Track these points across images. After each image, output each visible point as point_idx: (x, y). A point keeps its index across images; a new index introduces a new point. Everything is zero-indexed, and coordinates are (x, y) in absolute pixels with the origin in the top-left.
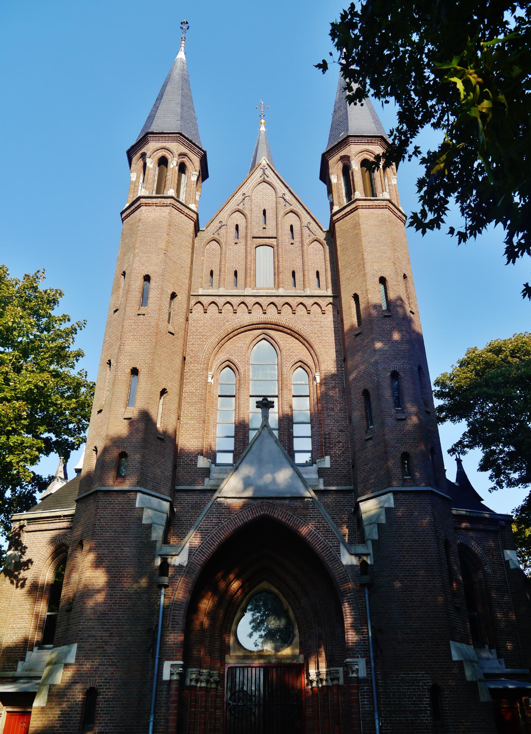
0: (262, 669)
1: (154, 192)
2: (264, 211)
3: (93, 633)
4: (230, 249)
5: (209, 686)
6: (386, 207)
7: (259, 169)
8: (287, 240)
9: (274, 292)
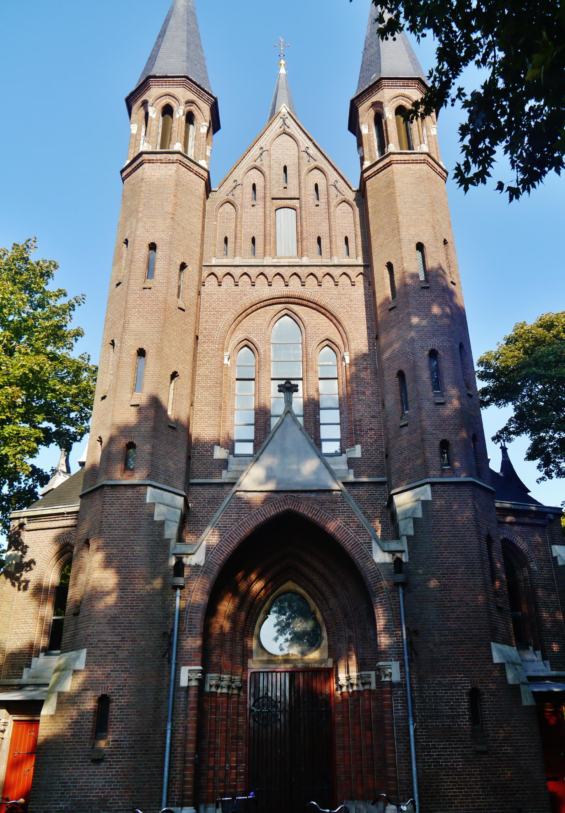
0: (287, 674)
1: (158, 147)
2: (285, 168)
3: (104, 637)
4: (247, 212)
8: (311, 201)
9: (297, 261)
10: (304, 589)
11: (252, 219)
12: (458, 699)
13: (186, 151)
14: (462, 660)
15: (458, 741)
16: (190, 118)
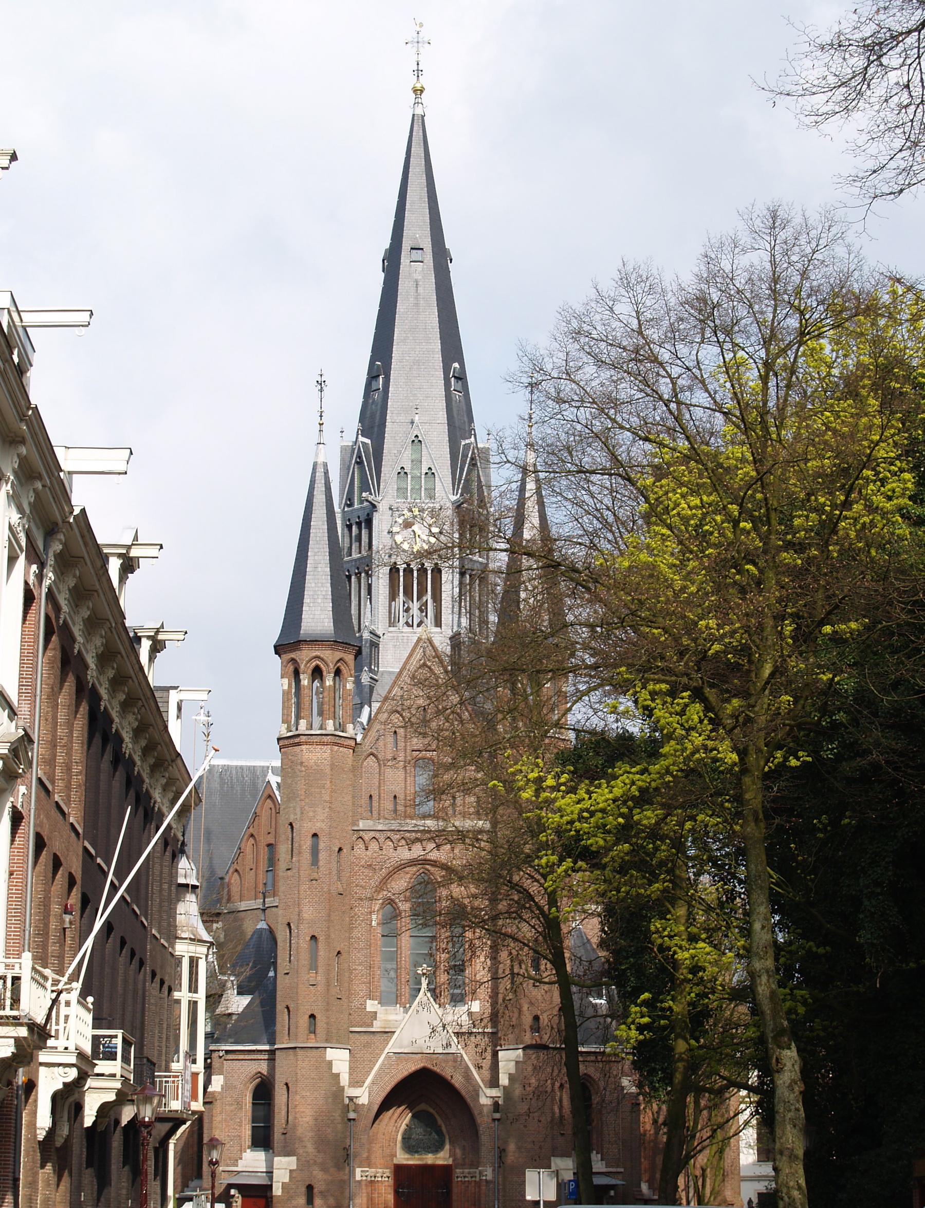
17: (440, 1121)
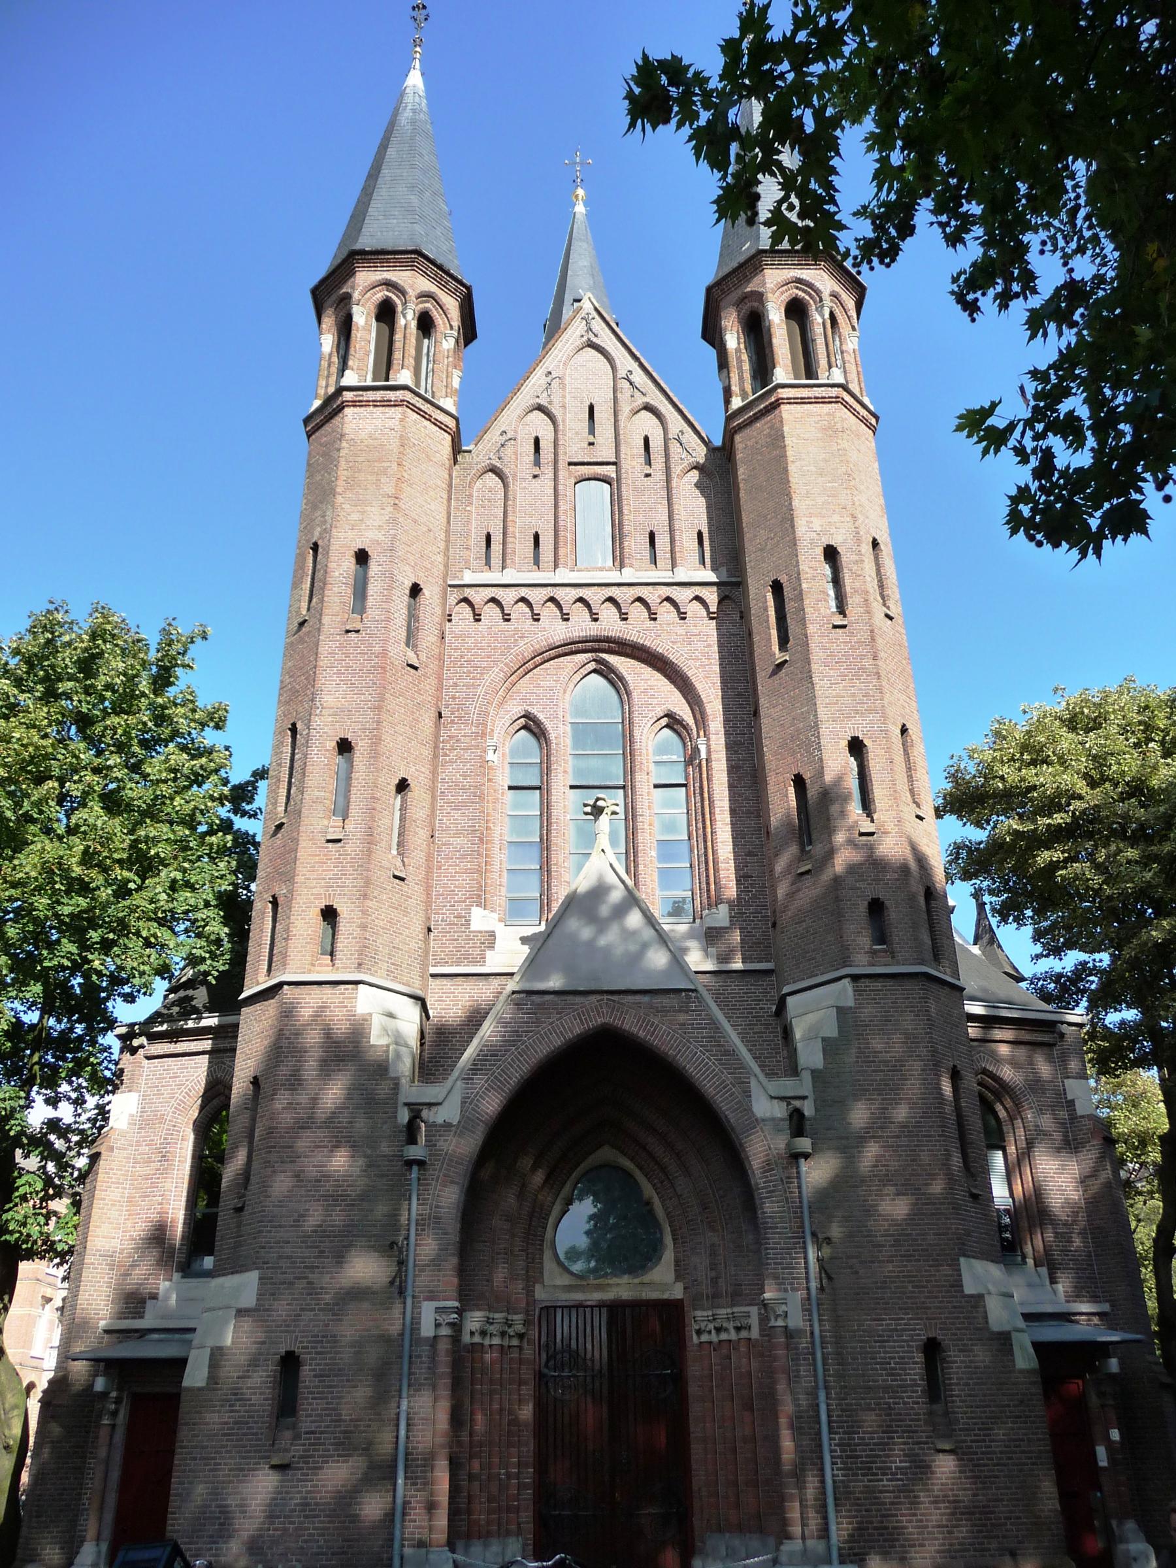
0: (604, 1310)
1: (370, 377)
2: (591, 408)
3: (288, 1250)
4: (525, 488)
5: (506, 1343)
6: (837, 400)
7: (578, 320)
8: (638, 468)
9: (614, 577)
10: (632, 1159)
11: (532, 498)
12: (903, 1358)
13: (418, 384)
14: (910, 1289)
15: (904, 1432)
16: (426, 324)
17: (648, 1190)
